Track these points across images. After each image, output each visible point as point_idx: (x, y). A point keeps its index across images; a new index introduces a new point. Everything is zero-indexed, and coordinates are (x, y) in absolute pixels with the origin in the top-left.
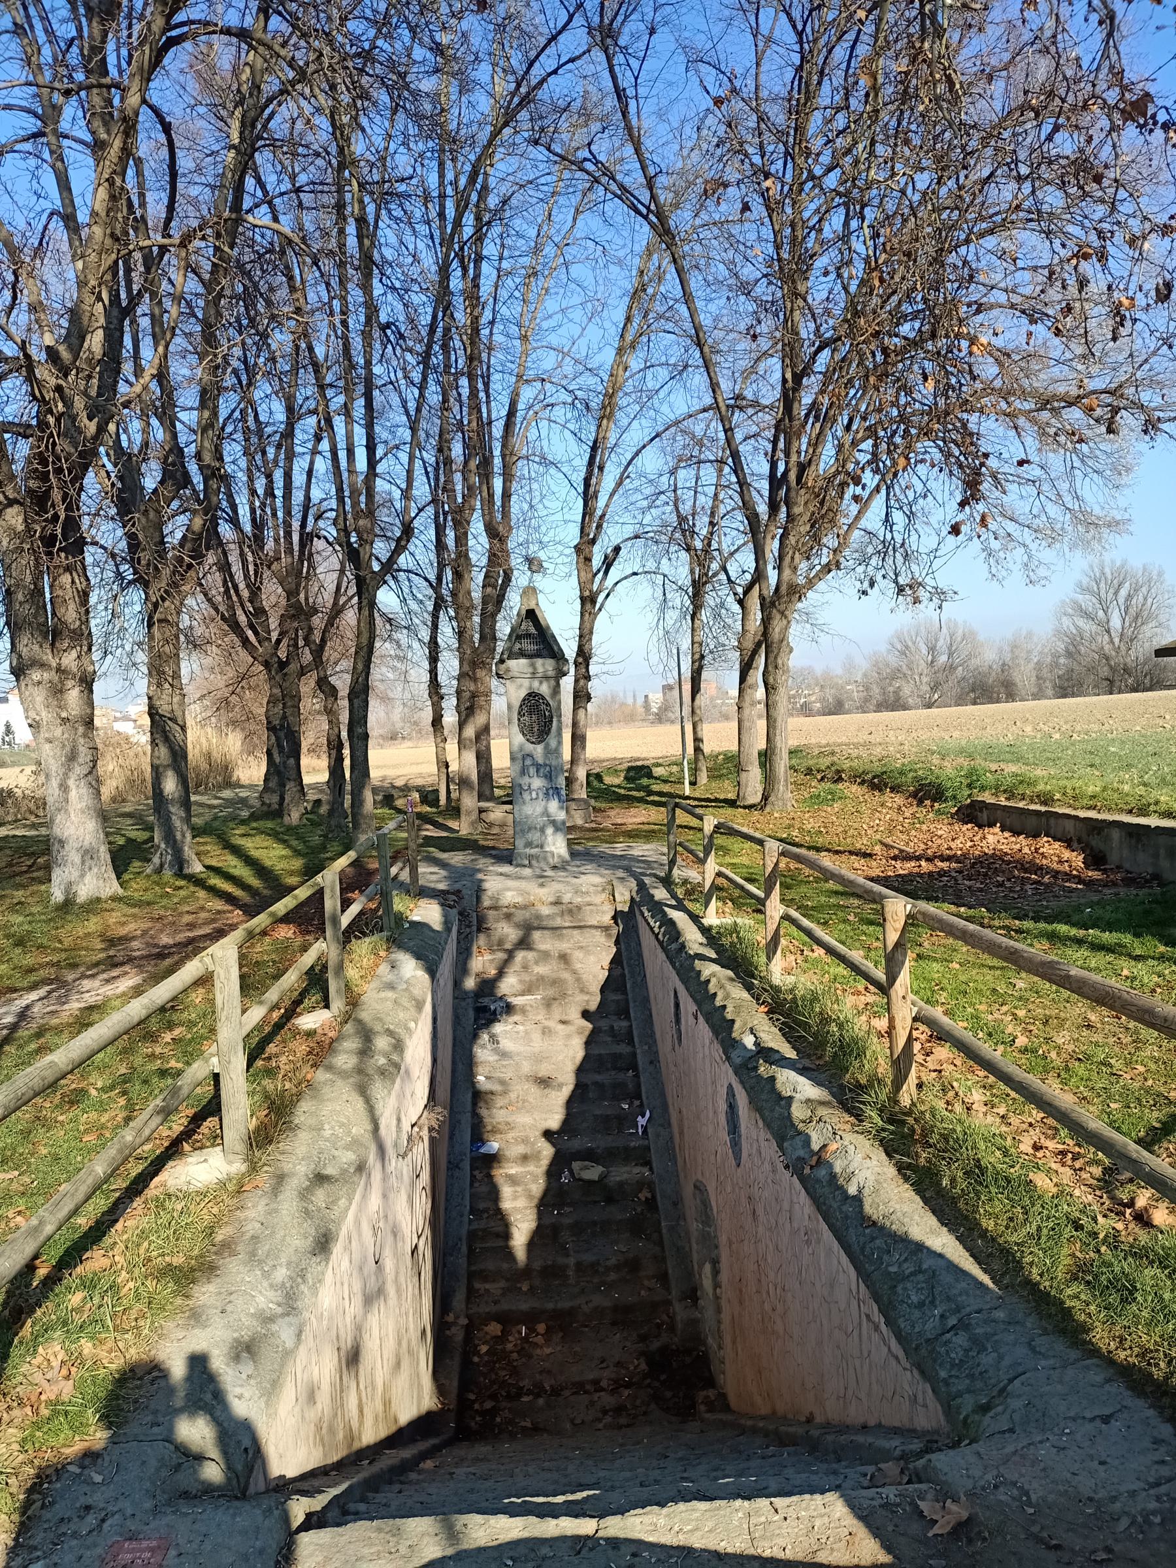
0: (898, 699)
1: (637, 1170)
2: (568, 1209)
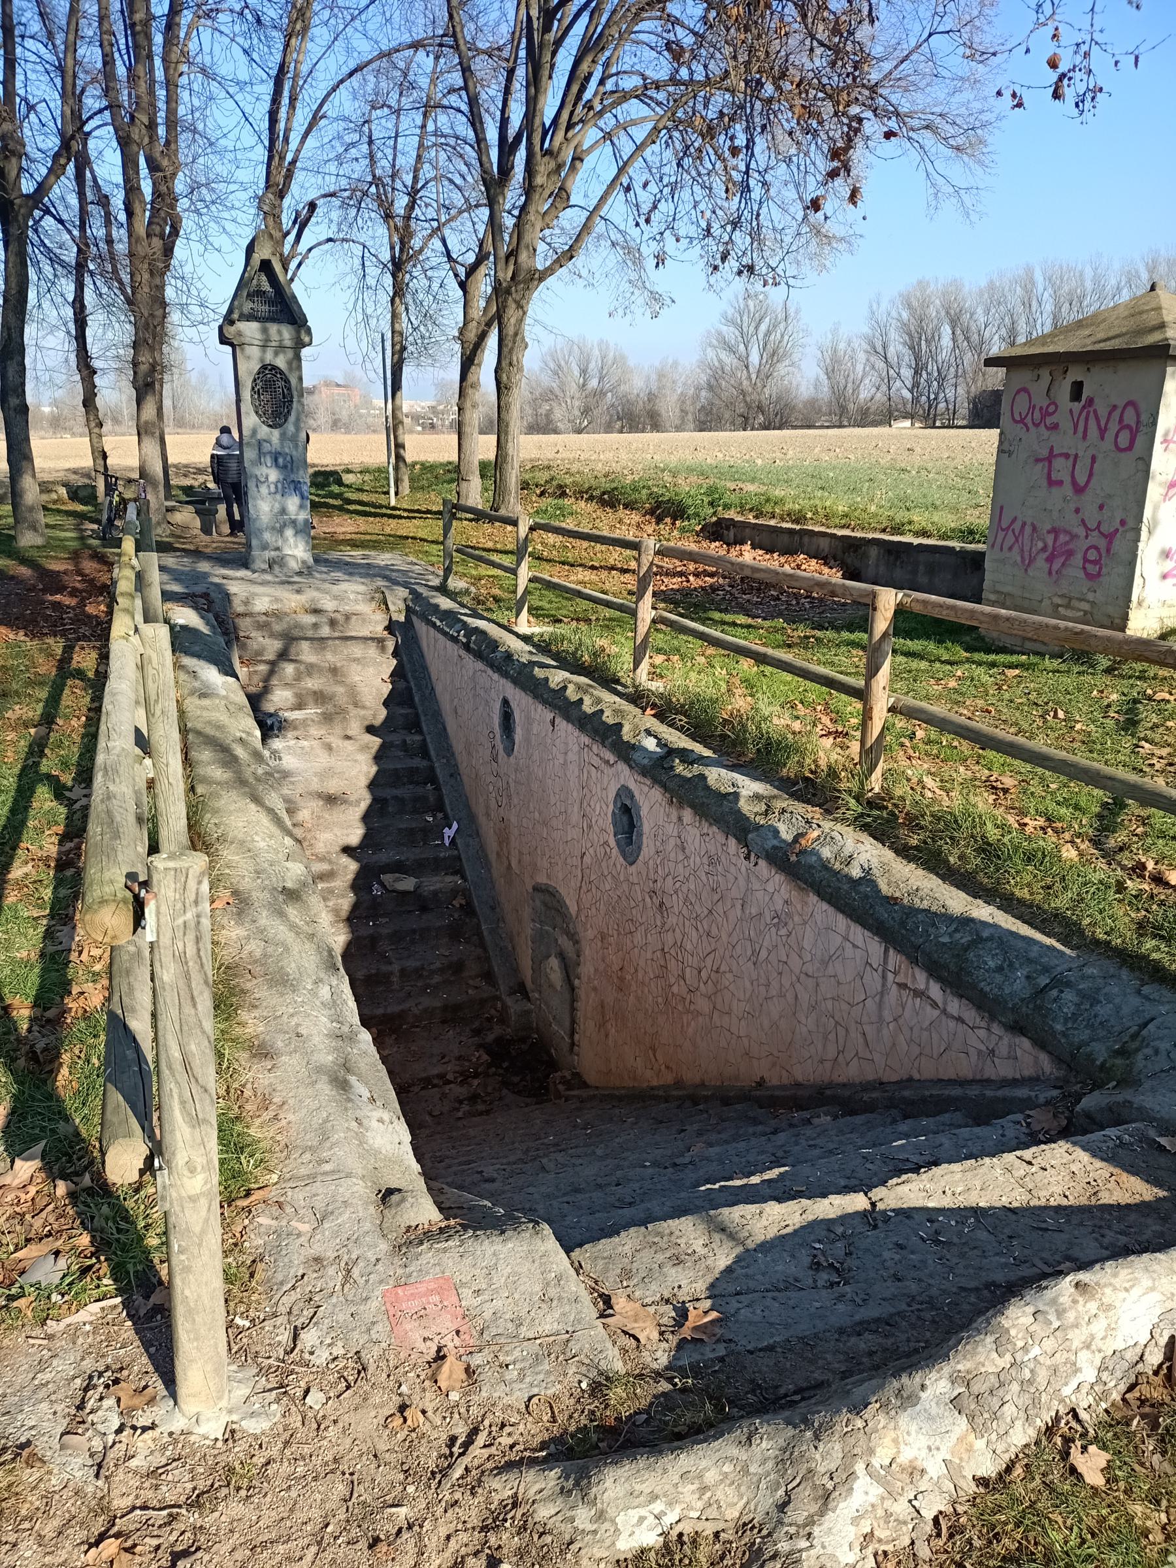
0: (549, 421)
1: (449, 879)
2: (384, 920)
